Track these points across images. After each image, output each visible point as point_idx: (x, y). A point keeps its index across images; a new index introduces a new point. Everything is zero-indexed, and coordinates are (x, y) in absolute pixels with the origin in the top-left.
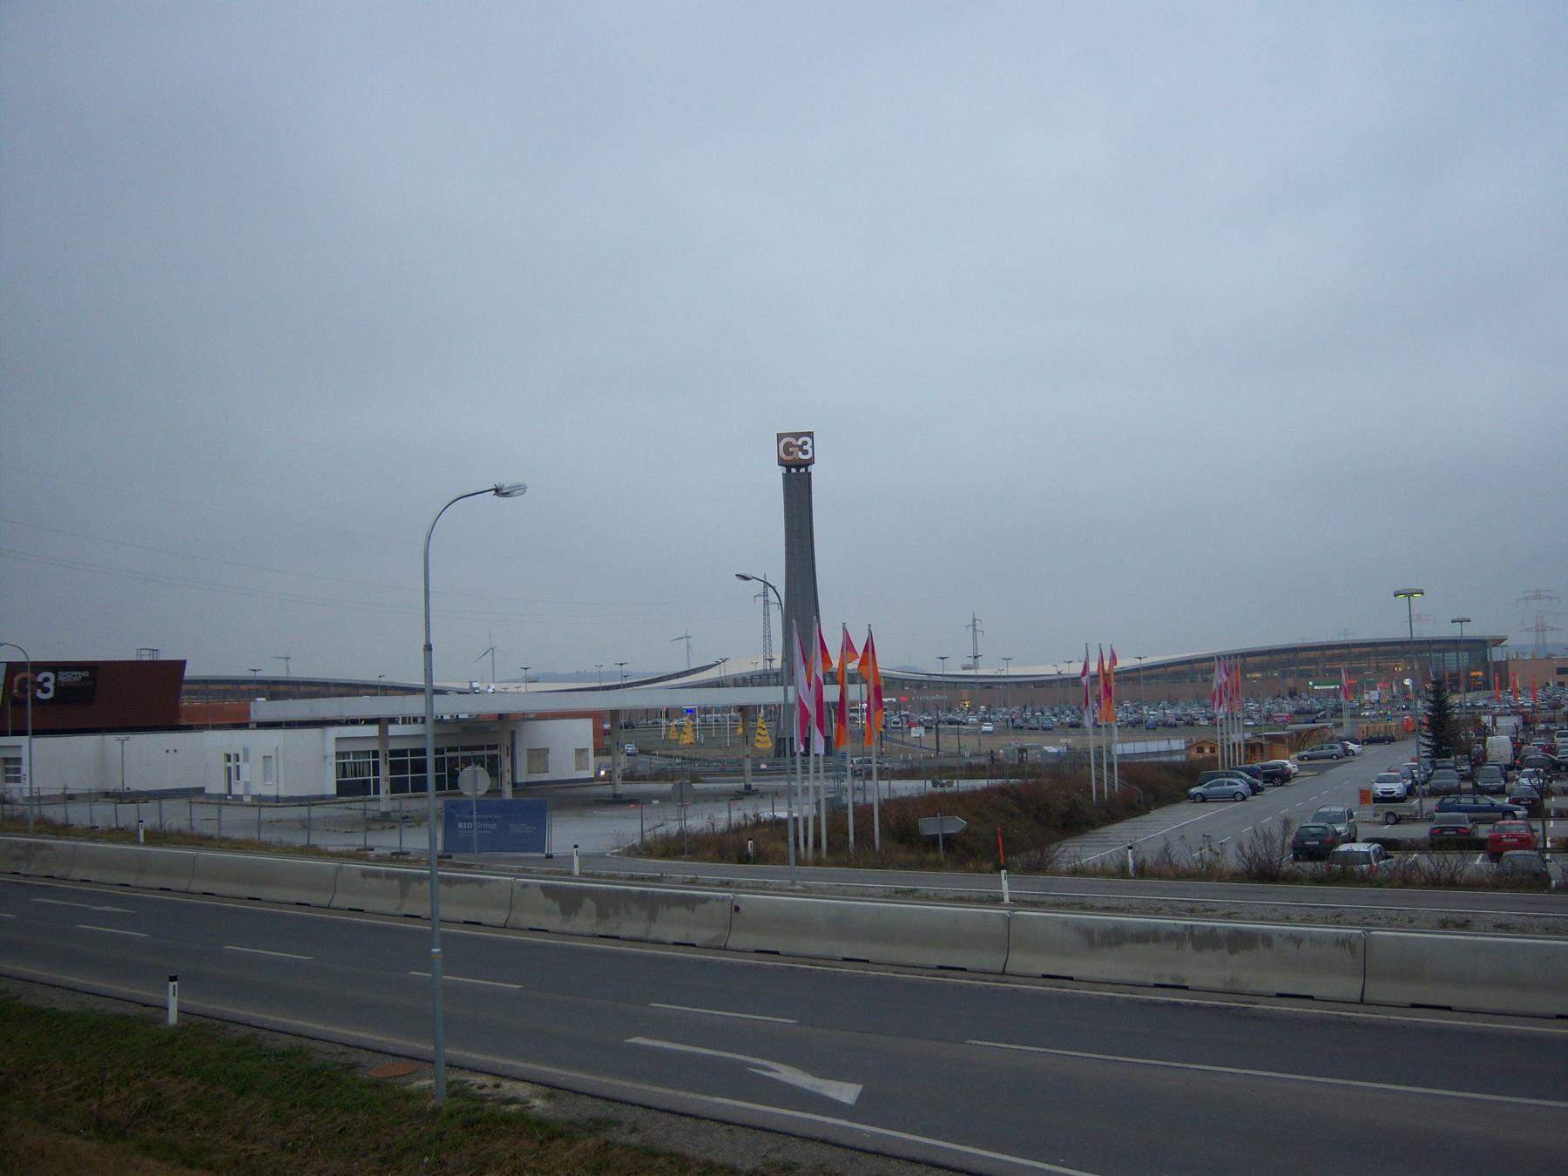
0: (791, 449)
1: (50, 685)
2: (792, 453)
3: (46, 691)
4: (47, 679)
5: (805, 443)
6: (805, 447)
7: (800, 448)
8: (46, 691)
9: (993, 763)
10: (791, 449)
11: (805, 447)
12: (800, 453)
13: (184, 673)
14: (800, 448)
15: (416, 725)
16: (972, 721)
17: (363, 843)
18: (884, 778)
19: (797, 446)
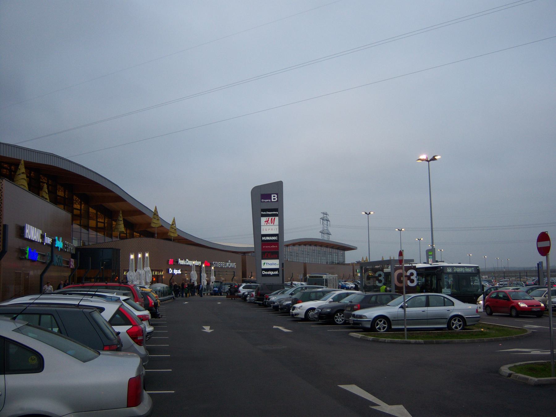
3: (412, 281)
5: (412, 274)
6: (412, 277)
7: (409, 278)
8: (412, 281)
11: (412, 277)
12: (409, 282)
14: (409, 278)
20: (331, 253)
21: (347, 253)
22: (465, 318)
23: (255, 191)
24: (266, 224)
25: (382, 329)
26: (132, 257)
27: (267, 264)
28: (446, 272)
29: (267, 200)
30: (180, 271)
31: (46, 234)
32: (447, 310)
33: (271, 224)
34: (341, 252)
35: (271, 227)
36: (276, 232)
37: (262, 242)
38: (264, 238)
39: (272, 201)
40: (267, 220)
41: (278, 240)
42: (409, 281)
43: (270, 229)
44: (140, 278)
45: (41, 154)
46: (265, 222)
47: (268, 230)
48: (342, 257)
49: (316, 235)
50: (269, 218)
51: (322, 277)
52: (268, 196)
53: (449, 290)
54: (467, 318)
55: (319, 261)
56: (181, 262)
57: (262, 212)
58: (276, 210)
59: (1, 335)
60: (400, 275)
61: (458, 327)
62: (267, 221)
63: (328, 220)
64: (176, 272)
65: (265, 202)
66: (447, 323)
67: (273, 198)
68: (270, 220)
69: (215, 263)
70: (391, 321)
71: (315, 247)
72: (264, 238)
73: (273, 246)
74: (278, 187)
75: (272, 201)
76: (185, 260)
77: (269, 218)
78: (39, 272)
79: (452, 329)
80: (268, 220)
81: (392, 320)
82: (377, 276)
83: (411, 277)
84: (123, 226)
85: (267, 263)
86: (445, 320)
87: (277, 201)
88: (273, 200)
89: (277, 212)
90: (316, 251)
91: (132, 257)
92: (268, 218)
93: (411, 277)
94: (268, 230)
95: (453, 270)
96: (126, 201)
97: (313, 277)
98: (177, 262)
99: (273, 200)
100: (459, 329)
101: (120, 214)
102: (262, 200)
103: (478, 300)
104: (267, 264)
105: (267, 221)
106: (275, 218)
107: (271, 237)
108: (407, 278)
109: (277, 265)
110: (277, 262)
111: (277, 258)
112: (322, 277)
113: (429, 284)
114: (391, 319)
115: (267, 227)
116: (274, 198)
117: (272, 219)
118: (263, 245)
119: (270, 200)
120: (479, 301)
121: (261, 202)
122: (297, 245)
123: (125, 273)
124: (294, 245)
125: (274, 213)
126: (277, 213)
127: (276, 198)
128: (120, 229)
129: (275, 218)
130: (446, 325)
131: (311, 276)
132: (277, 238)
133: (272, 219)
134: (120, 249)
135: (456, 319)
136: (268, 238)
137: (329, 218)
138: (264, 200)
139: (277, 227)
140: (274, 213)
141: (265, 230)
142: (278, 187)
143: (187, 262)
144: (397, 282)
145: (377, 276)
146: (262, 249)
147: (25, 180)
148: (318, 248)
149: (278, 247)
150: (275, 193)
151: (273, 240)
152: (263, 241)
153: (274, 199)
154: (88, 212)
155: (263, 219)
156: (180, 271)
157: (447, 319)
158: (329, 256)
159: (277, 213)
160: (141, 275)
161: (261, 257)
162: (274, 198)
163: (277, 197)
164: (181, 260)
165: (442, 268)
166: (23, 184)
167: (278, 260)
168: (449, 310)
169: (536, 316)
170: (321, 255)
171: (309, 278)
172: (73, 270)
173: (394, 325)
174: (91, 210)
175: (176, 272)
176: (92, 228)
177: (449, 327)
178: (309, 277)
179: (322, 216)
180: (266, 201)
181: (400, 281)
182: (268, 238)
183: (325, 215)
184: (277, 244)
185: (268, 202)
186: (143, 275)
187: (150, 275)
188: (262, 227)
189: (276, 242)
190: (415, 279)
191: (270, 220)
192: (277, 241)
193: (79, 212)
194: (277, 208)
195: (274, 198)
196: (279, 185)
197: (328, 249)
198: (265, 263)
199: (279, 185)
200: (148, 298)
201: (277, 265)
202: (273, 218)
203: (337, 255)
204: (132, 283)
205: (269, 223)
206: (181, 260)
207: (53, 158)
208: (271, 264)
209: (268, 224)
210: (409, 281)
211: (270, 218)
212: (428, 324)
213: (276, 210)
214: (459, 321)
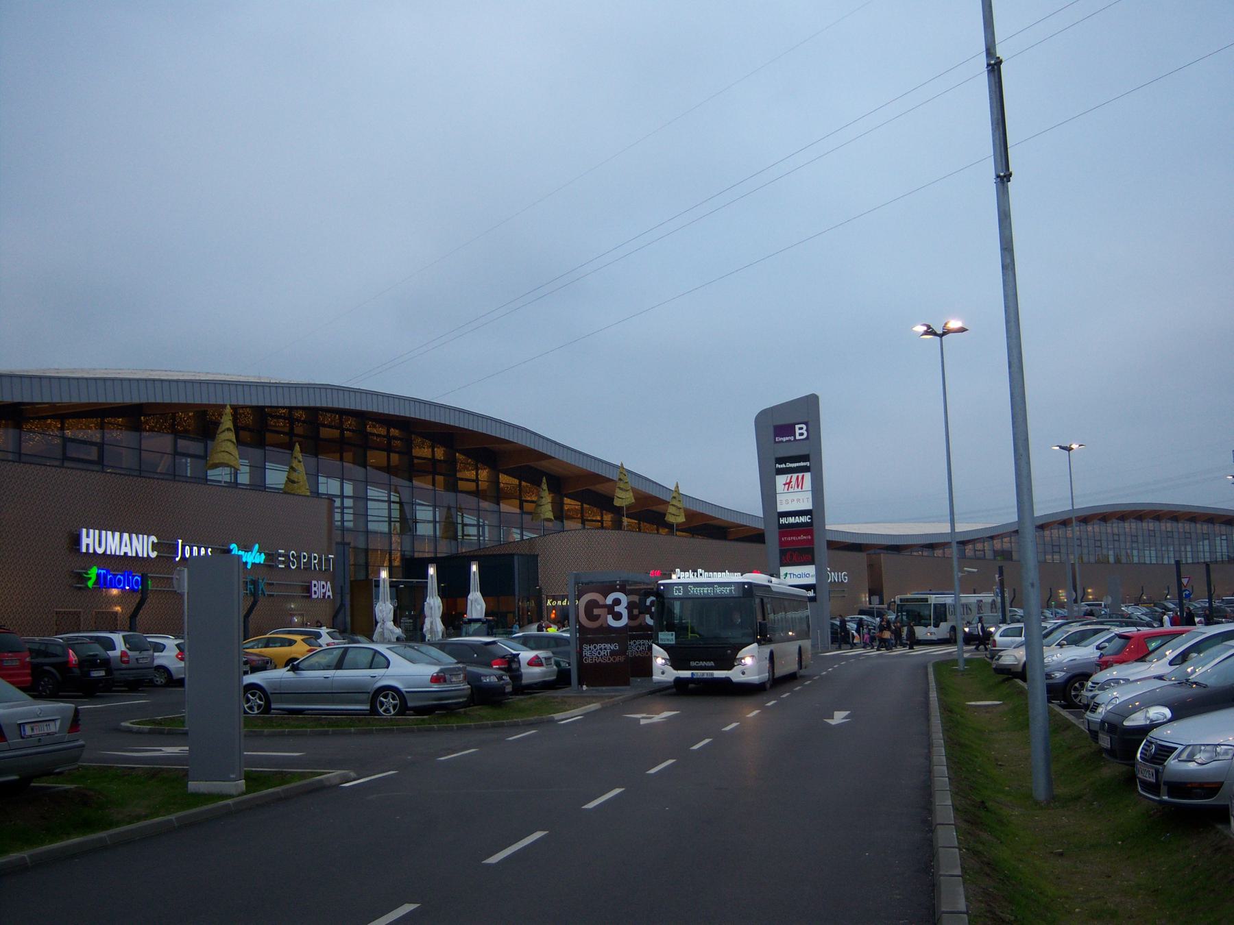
0: (596, 611)
1: (622, 609)
2: (598, 617)
3: (618, 616)
4: (617, 602)
5: (617, 602)
6: (617, 609)
7: (610, 609)
8: (618, 616)
9: (462, 514)
10: (596, 611)
11: (617, 609)
12: (610, 617)
13: (687, 678)
14: (610, 609)
15: (615, 534)
16: (1192, 670)
17: (25, 436)
18: (1078, 634)
19: (605, 606)
20: (1149, 536)
22: (405, 694)
23: (763, 418)
24: (786, 491)
25: (256, 708)
27: (792, 575)
28: (672, 596)
29: (787, 438)
31: (180, 541)
32: (325, 678)
33: (796, 489)
35: (795, 496)
36: (808, 506)
37: (779, 528)
38: (783, 521)
39: (797, 438)
40: (788, 481)
42: (611, 616)
43: (795, 500)
44: (431, 613)
45: (329, 391)
46: (785, 485)
47: (790, 501)
50: (792, 477)
51: (926, 600)
52: (788, 430)
53: (672, 635)
54: (407, 692)
55: (1183, 553)
57: (777, 465)
58: (805, 458)
60: (592, 605)
61: (383, 708)
62: (789, 483)
65: (782, 442)
66: (369, 701)
67: (798, 432)
68: (794, 480)
70: (269, 694)
72: (783, 521)
73: (802, 537)
74: (808, 407)
75: (797, 438)
76: (695, 571)
77: (792, 477)
79: (379, 714)
80: (791, 482)
81: (272, 693)
82: (611, 603)
83: (615, 607)
84: (549, 507)
85: (790, 574)
86: (364, 697)
87: (807, 438)
88: (798, 437)
89: (808, 463)
90: (1122, 538)
92: (790, 476)
93: (615, 607)
94: (790, 501)
95: (686, 591)
96: (554, 458)
97: (907, 600)
99: (798, 437)
100: (246, 706)
101: (543, 484)
102: (777, 438)
103: (738, 657)
104: (792, 575)
105: (789, 483)
106: (803, 476)
107: (797, 517)
108: (606, 610)
109: (812, 576)
110: (811, 569)
111: (810, 562)
112: (926, 600)
113: (493, 620)
114: (269, 692)
115: (789, 497)
116: (801, 431)
117: (798, 477)
118: (782, 535)
119: (792, 438)
120: (743, 658)
121: (775, 442)
123: (549, 602)
125: (802, 464)
126: (808, 464)
127: (804, 431)
128: (542, 515)
129: (803, 476)
130: (369, 704)
131: (904, 599)
132: (809, 519)
133: (798, 477)
134: (538, 555)
135: (388, 694)
136: (791, 520)
138: (781, 439)
139: (809, 495)
140: (802, 464)
141: (784, 502)
142: (808, 407)
143: (701, 575)
144: (588, 622)
145: (611, 603)
146: (781, 543)
147: (233, 442)
148: (1168, 526)
149: (812, 539)
150: (802, 421)
151: (802, 524)
152: (781, 526)
153: (801, 434)
154: (498, 483)
155: (781, 480)
157: (369, 693)
159: (808, 464)
160: (433, 608)
161: (778, 561)
162: (801, 431)
163: (807, 430)
164: (681, 571)
165: (662, 587)
166: (227, 450)
168: (327, 677)
169: (127, 689)
171: (899, 603)
173: (276, 702)
174: (504, 479)
177: (373, 711)
178: (901, 602)
180: (784, 439)
181: (590, 616)
182: (791, 520)
184: (810, 532)
185: (790, 441)
186: (437, 608)
187: (479, 607)
189: (807, 528)
190: (625, 613)
191: (794, 480)
192: (810, 524)
193: (474, 484)
194: (807, 453)
195: (801, 431)
196: (811, 402)
197: (1199, 526)
198: (787, 574)
199: (811, 402)
200: (68, 652)
201: (812, 576)
202: (800, 475)
204: (384, 624)
205: (792, 488)
206: (681, 571)
207: (353, 397)
208: (800, 576)
209: (791, 490)
210: (611, 616)
211: (795, 476)
212: (333, 703)
213: (805, 458)
214: (394, 698)
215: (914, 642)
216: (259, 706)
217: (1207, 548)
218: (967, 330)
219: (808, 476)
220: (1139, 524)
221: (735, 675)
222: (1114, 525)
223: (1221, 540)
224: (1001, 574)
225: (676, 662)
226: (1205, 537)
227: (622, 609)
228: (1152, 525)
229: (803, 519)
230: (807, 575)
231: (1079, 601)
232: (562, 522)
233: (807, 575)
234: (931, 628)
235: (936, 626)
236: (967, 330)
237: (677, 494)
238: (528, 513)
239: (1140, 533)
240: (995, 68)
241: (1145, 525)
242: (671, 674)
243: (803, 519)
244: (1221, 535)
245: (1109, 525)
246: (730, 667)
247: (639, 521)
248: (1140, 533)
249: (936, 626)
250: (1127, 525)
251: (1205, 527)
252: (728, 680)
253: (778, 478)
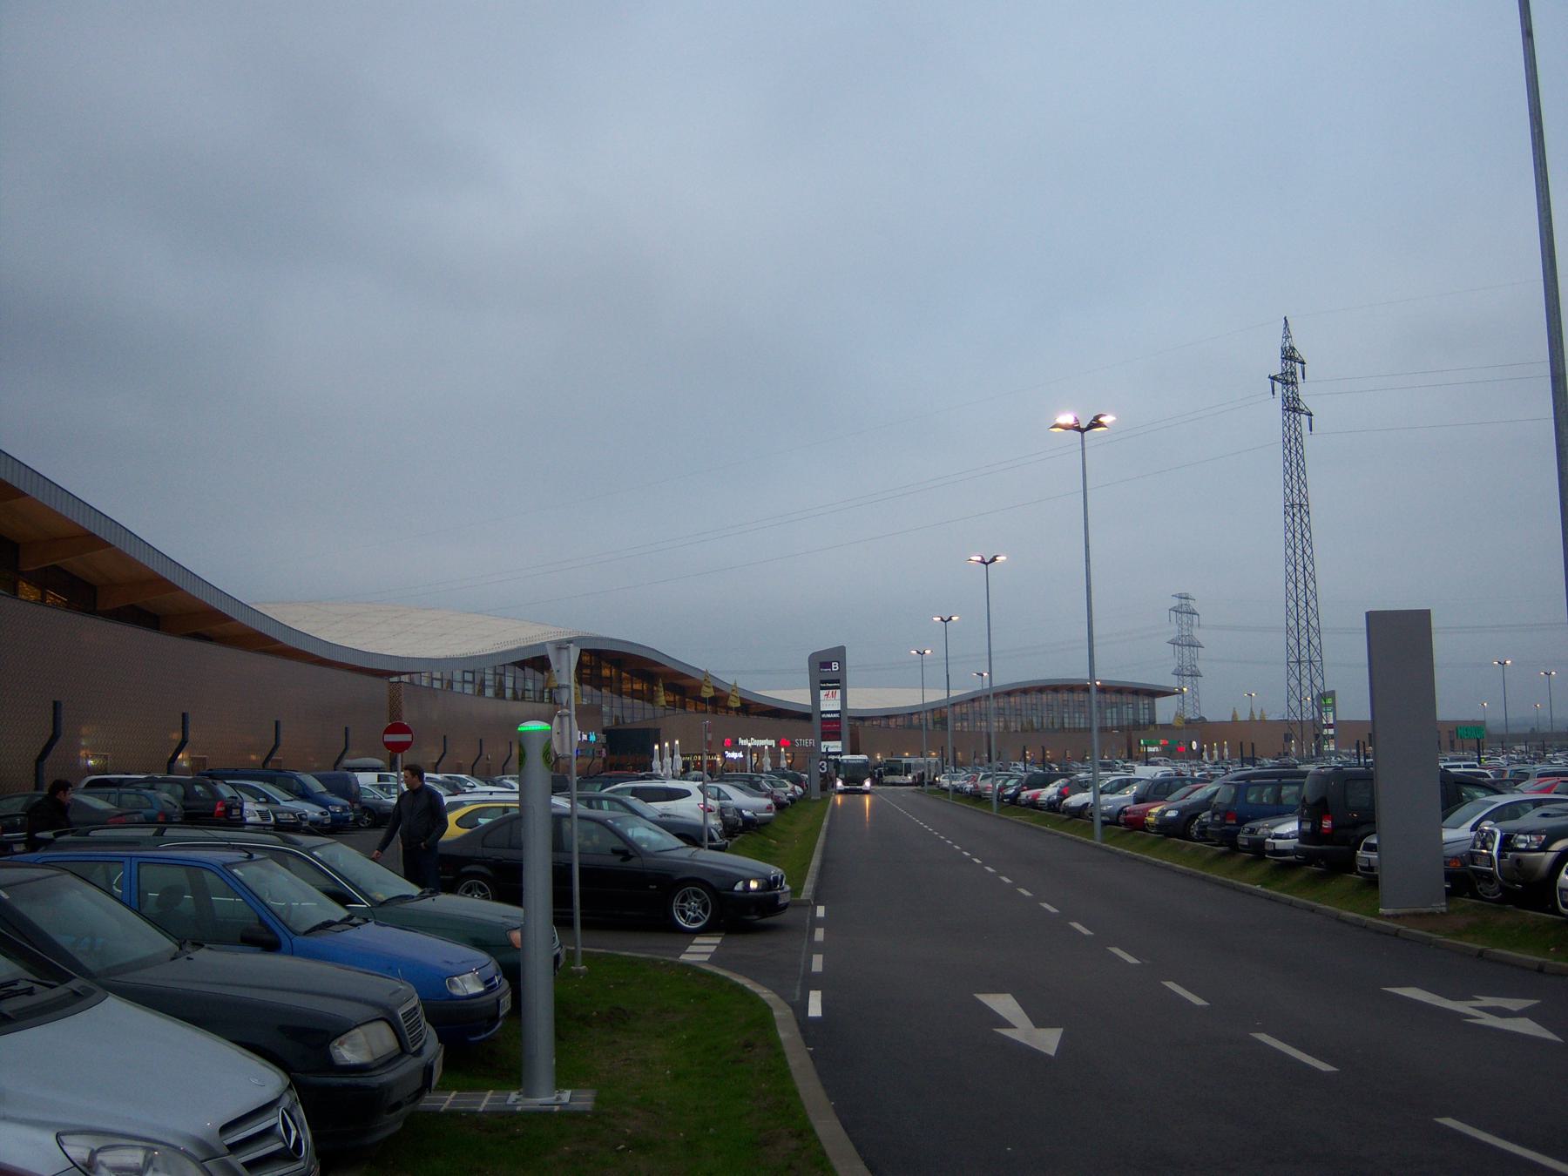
3: (823, 769)
4: (823, 764)
5: (823, 764)
8: (823, 769)
21: (1159, 701)
23: (812, 658)
26: (656, 747)
30: (741, 753)
34: (1143, 702)
35: (832, 702)
38: (823, 716)
41: (840, 718)
48: (1146, 711)
49: (1073, 669)
56: (742, 742)
59: (8, 1162)
63: (1193, 613)
64: (734, 755)
69: (799, 742)
71: (1071, 694)
72: (823, 716)
74: (839, 654)
78: (595, 761)
87: (839, 670)
91: (656, 747)
98: (738, 742)
115: (828, 703)
118: (822, 723)
122: (1034, 693)
124: (1009, 694)
136: (829, 716)
137: (1193, 605)
142: (839, 654)
146: (822, 729)
155: (823, 693)
156: (741, 753)
158: (1013, 719)
161: (820, 739)
162: (835, 666)
167: (840, 742)
170: (1071, 709)
172: (604, 758)
174: (624, 675)
175: (734, 755)
176: (626, 693)
179: (1176, 602)
182: (829, 716)
183: (1184, 601)
184: (840, 723)
188: (821, 703)
197: (1108, 696)
203: (1132, 708)
213: (838, 681)
215: (882, 784)
216: (368, 822)
217: (1115, 716)
218: (1014, 1027)
219: (838, 691)
220: (1055, 695)
221: (862, 787)
222: (1034, 696)
223: (1128, 708)
224: (942, 750)
225: (844, 784)
226: (1112, 705)
227: (824, 766)
228: (1066, 696)
229: (835, 715)
230: (837, 747)
231: (993, 759)
232: (524, 670)
233: (837, 747)
234: (903, 777)
235: (906, 775)
236: (1014, 1027)
237: (735, 688)
238: (650, 698)
239: (1055, 703)
240: (948, 676)
241: (1060, 695)
242: (843, 787)
243: (835, 715)
244: (1128, 704)
245: (1028, 696)
246: (861, 785)
247: (632, 676)
248: (1055, 703)
249: (906, 775)
250: (1044, 696)
251: (1114, 697)
252: (861, 789)
253: (821, 692)
